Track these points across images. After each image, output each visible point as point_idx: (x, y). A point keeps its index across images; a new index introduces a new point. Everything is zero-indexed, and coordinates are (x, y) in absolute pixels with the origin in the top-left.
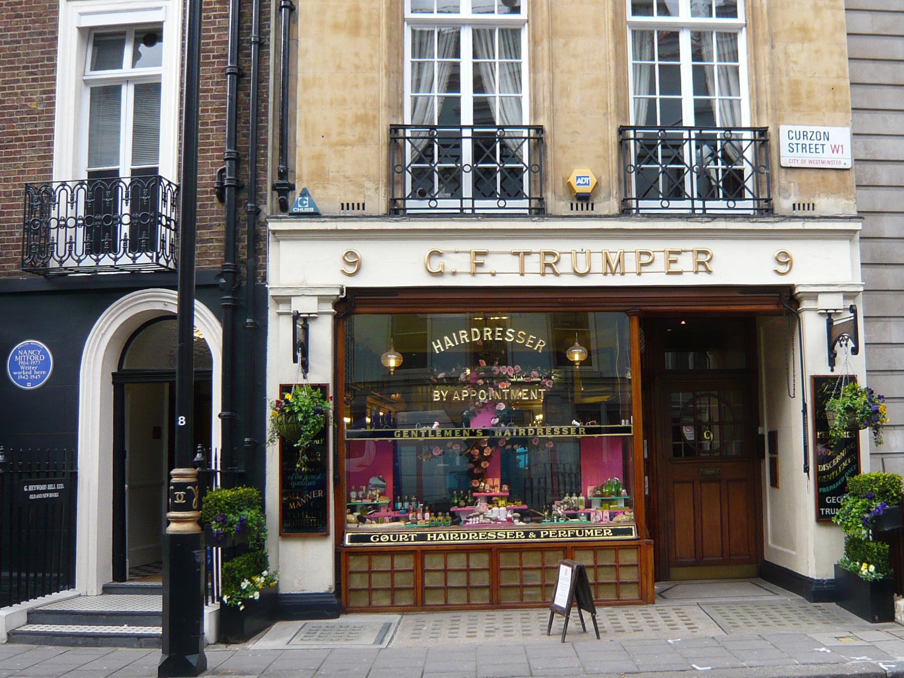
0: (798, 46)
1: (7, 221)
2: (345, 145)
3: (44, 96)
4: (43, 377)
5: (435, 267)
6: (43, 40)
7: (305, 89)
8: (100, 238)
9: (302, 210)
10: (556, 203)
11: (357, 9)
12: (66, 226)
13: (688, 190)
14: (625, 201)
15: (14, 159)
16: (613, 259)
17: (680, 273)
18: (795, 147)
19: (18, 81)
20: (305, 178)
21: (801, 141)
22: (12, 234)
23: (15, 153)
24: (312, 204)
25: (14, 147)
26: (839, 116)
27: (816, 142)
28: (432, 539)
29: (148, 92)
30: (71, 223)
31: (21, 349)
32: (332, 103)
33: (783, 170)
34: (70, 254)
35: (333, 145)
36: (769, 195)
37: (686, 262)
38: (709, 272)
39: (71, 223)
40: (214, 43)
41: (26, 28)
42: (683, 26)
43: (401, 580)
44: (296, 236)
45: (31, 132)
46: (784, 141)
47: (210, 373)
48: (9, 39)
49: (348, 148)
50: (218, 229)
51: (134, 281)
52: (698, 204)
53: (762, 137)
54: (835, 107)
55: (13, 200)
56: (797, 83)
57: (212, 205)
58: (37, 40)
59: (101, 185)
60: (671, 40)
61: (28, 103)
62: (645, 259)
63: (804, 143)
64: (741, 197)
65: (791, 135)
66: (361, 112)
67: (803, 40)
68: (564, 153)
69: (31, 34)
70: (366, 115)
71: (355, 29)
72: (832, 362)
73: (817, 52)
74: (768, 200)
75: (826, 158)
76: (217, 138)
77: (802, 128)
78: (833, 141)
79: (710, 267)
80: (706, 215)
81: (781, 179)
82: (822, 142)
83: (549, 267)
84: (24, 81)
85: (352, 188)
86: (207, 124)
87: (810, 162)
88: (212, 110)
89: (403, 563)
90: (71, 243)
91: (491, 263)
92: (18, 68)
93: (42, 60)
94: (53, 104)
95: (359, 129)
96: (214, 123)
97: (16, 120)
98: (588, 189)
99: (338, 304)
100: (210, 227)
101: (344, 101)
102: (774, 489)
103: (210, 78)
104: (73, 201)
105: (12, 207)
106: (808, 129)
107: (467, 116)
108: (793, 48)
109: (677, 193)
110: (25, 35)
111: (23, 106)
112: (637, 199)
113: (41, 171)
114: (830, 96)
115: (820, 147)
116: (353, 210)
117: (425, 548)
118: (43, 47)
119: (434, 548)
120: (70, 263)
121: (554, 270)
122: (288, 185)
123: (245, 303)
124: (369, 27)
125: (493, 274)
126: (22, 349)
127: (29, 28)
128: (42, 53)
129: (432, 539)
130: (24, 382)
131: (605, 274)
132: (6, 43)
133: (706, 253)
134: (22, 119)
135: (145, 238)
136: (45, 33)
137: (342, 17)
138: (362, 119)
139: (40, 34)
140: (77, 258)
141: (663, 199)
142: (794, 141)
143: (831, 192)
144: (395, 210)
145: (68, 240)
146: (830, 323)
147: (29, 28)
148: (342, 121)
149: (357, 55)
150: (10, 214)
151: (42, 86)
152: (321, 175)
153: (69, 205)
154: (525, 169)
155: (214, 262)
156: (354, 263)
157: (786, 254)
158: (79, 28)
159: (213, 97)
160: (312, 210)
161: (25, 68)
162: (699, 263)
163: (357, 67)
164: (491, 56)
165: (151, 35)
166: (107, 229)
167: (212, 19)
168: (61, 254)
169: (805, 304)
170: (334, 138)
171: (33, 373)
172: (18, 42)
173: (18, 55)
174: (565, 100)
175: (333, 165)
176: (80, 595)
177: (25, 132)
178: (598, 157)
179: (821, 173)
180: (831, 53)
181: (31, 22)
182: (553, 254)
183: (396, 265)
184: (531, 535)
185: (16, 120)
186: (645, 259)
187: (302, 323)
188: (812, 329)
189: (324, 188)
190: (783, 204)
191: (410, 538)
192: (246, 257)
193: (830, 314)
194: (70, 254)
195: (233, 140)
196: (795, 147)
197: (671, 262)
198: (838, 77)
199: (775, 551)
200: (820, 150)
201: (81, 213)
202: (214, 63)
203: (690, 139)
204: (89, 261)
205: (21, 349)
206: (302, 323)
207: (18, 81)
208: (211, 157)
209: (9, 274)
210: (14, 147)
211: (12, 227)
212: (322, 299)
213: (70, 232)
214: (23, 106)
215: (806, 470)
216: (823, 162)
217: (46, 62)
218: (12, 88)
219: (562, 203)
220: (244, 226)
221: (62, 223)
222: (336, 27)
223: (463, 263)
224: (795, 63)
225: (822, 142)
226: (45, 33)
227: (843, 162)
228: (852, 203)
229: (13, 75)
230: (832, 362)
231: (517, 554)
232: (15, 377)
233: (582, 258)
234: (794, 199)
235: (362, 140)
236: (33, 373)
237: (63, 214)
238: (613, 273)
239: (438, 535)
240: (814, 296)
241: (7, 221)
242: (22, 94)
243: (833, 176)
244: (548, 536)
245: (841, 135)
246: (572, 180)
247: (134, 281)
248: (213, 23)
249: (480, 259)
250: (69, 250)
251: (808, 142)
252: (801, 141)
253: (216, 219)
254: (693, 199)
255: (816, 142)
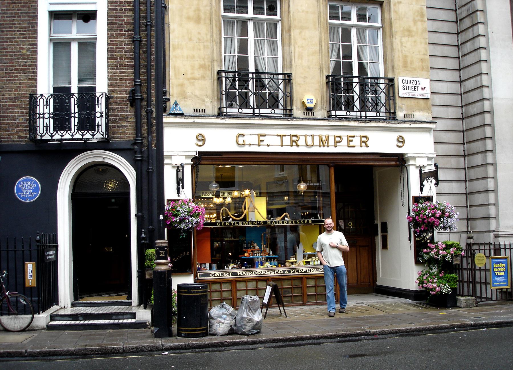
0: (407, 39)
1: (11, 113)
2: (195, 79)
3: (30, 47)
4: (35, 196)
5: (241, 140)
6: (28, 16)
7: (174, 49)
8: (61, 123)
9: (176, 112)
10: (298, 112)
11: (198, 10)
12: (44, 117)
13: (251, 103)
14: (220, 109)
15: (14, 80)
16: (324, 138)
17: (354, 147)
18: (405, 87)
19: (14, 38)
20: (175, 95)
21: (408, 85)
22: (14, 120)
23: (14, 77)
24: (180, 110)
25: (14, 73)
26: (424, 73)
27: (415, 85)
28: (240, 275)
29: (87, 46)
30: (47, 116)
31: (22, 181)
32: (187, 58)
33: (400, 98)
34: (47, 132)
35: (188, 79)
36: (291, 107)
37: (356, 141)
38: (367, 146)
39: (47, 116)
40: (125, 23)
41: (18, 10)
42: (353, 26)
43: (225, 295)
44: (174, 125)
45: (23, 66)
46: (401, 85)
47: (129, 194)
48: (9, 15)
49: (196, 81)
50: (130, 120)
51: (85, 146)
52: (257, 111)
53: (391, 82)
54: (423, 69)
55: (14, 102)
56: (406, 57)
57: (127, 108)
58: (25, 17)
59: (61, 95)
60: (70, 16)
61: (21, 50)
62: (338, 139)
63: (411, 85)
64: (278, 108)
65: (404, 82)
66: (202, 63)
67: (409, 36)
68: (300, 87)
69: (22, 13)
70: (205, 65)
71: (198, 20)
72: (422, 190)
73: (415, 42)
74: (291, 110)
75: (419, 93)
76: (128, 73)
77: (408, 79)
78: (423, 85)
79: (368, 143)
80: (260, 116)
81: (399, 102)
82: (417, 85)
83: (294, 142)
84: (18, 38)
85: (199, 101)
86: (122, 65)
87: (412, 95)
88: (125, 59)
89: (225, 287)
90: (47, 126)
91: (267, 140)
92: (14, 31)
93: (29, 27)
94: (36, 51)
95: (201, 72)
96: (126, 65)
97: (14, 59)
98: (312, 105)
99: (194, 159)
100: (126, 119)
101: (193, 57)
102: (385, 250)
103: (123, 41)
104: (47, 105)
105: (14, 105)
106: (411, 79)
107: (355, 72)
108: (404, 40)
109: (245, 104)
110: (18, 13)
111: (19, 52)
112: (226, 108)
113: (30, 87)
114: (421, 63)
115: (416, 88)
116: (200, 113)
117: (237, 279)
118: (29, 20)
119: (241, 279)
120: (47, 137)
121: (366, 144)
122: (166, 99)
123: (149, 159)
124: (205, 19)
125: (268, 146)
126: (23, 181)
127: (20, 10)
128: (28, 23)
129: (240, 275)
130: (25, 199)
131: (320, 146)
132: (7, 17)
133: (366, 137)
134: (18, 59)
135: (87, 123)
136: (29, 13)
137: (191, 14)
138: (202, 66)
139: (27, 13)
140: (50, 134)
141: (239, 108)
142: (405, 85)
143: (421, 109)
144: (220, 114)
145: (45, 125)
146: (421, 171)
147: (20, 10)
148: (193, 68)
149: (199, 33)
150: (12, 109)
151: (29, 41)
152: (184, 95)
153: (45, 106)
154: (250, 93)
155: (129, 137)
156: (201, 139)
157: (403, 138)
158: (49, 12)
159: (126, 52)
160: (181, 112)
161: (18, 31)
162: (293, 141)
163: (200, 40)
164: (258, 36)
165: (88, 16)
166: (88, 119)
167: (123, 11)
168: (41, 132)
169: (411, 162)
170: (189, 76)
171: (30, 193)
172: (14, 17)
173: (14, 24)
174: (300, 61)
175: (189, 90)
176: (61, 308)
177: (20, 66)
178: (316, 89)
179: (417, 100)
180: (421, 43)
181: (21, 6)
182: (296, 136)
183: (222, 140)
184: (286, 272)
185: (14, 59)
186: (338, 139)
187: (180, 169)
188: (414, 175)
189: (185, 101)
190: (400, 115)
191: (229, 274)
192: (146, 135)
193: (421, 167)
194: (47, 132)
195: (137, 74)
196: (405, 87)
197: (350, 141)
198: (424, 54)
199: (383, 279)
200: (416, 89)
201: (52, 111)
202: (125, 34)
203: (253, 78)
204: (57, 136)
205: (22, 181)
206: (180, 169)
207: (14, 38)
208: (125, 83)
209: (14, 141)
210: (14, 73)
211: (14, 116)
212: (187, 156)
213: (46, 121)
214: (19, 52)
215: (410, 240)
216: (418, 95)
217: (31, 29)
218: (12, 42)
219: (300, 112)
220: (144, 119)
221: (41, 116)
222: (189, 18)
223: (254, 140)
224: (405, 47)
225: (417, 85)
226: (29, 13)
227: (426, 95)
228: (430, 114)
229: (12, 35)
230: (422, 190)
231: (280, 281)
232: (20, 196)
233: (309, 139)
234: (405, 112)
235: (203, 77)
236: (30, 193)
237: (41, 111)
238: (324, 146)
239: (242, 273)
240: (414, 158)
241: (11, 113)
242: (17, 45)
243: (421, 102)
244: (294, 272)
245: (425, 83)
246: (305, 101)
247: (85, 146)
248: (124, 13)
249: (262, 138)
250: (46, 129)
251: (411, 85)
252: (408, 85)
253: (129, 115)
254: (254, 109)
255: (415, 85)
